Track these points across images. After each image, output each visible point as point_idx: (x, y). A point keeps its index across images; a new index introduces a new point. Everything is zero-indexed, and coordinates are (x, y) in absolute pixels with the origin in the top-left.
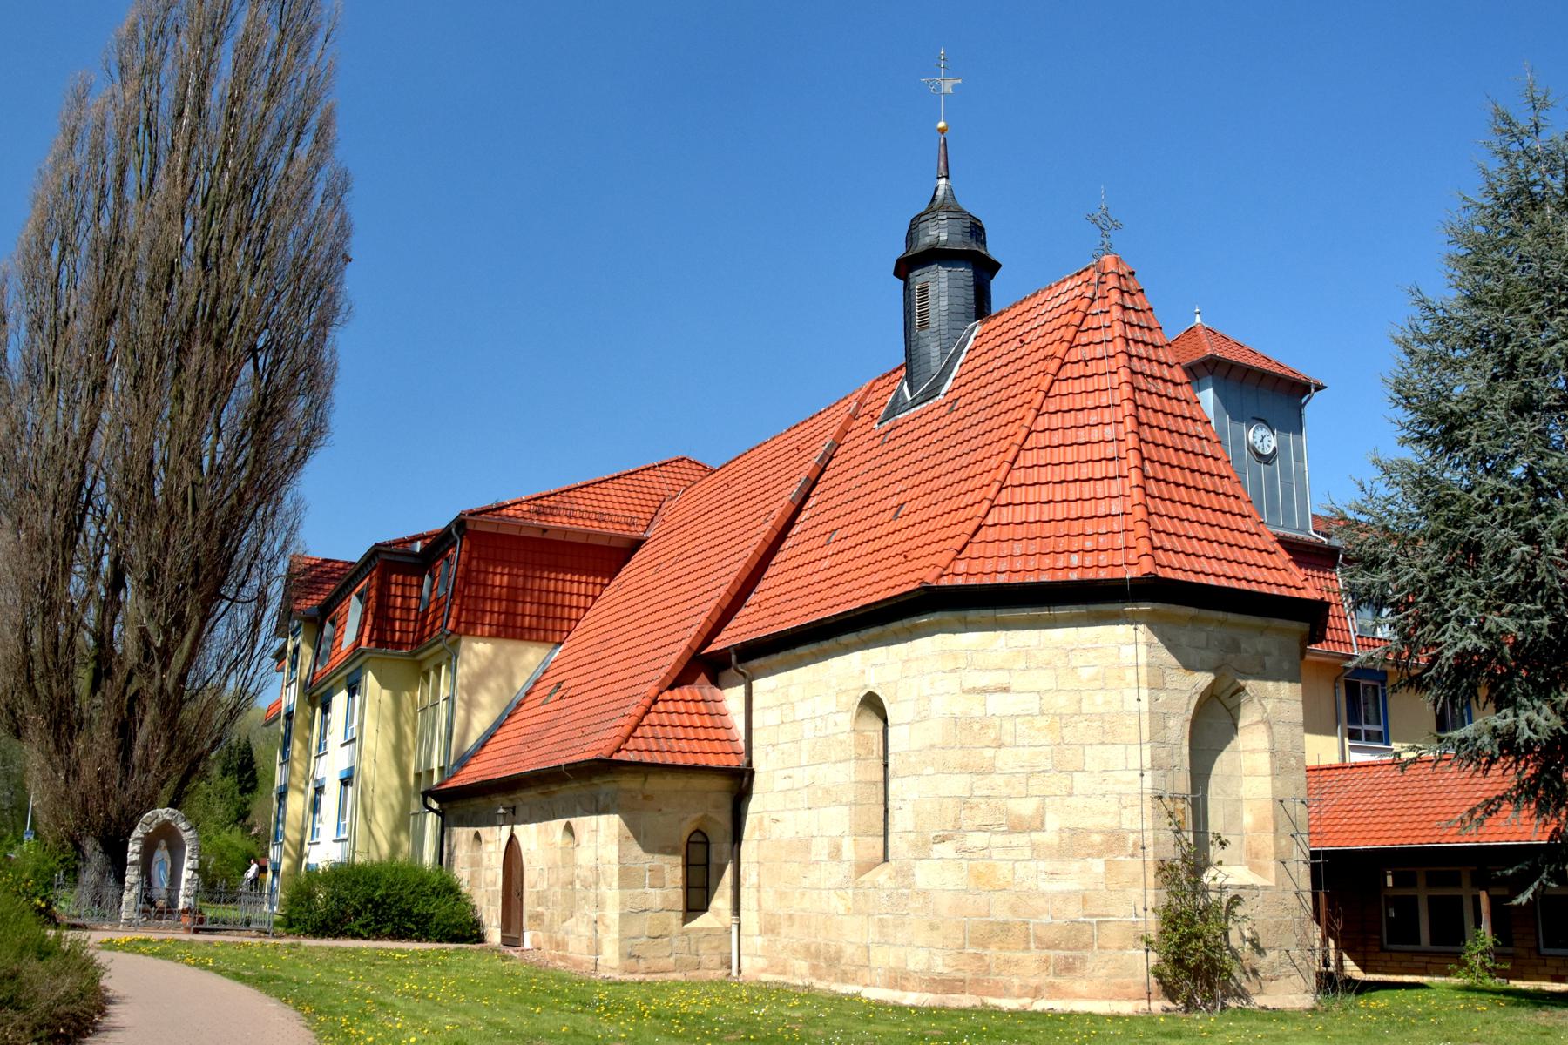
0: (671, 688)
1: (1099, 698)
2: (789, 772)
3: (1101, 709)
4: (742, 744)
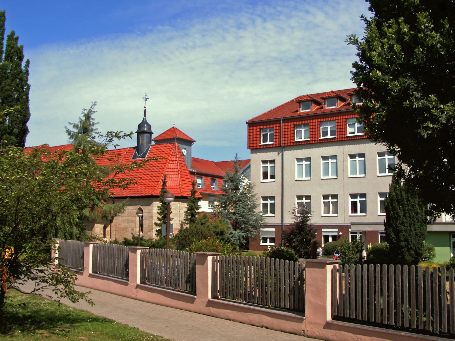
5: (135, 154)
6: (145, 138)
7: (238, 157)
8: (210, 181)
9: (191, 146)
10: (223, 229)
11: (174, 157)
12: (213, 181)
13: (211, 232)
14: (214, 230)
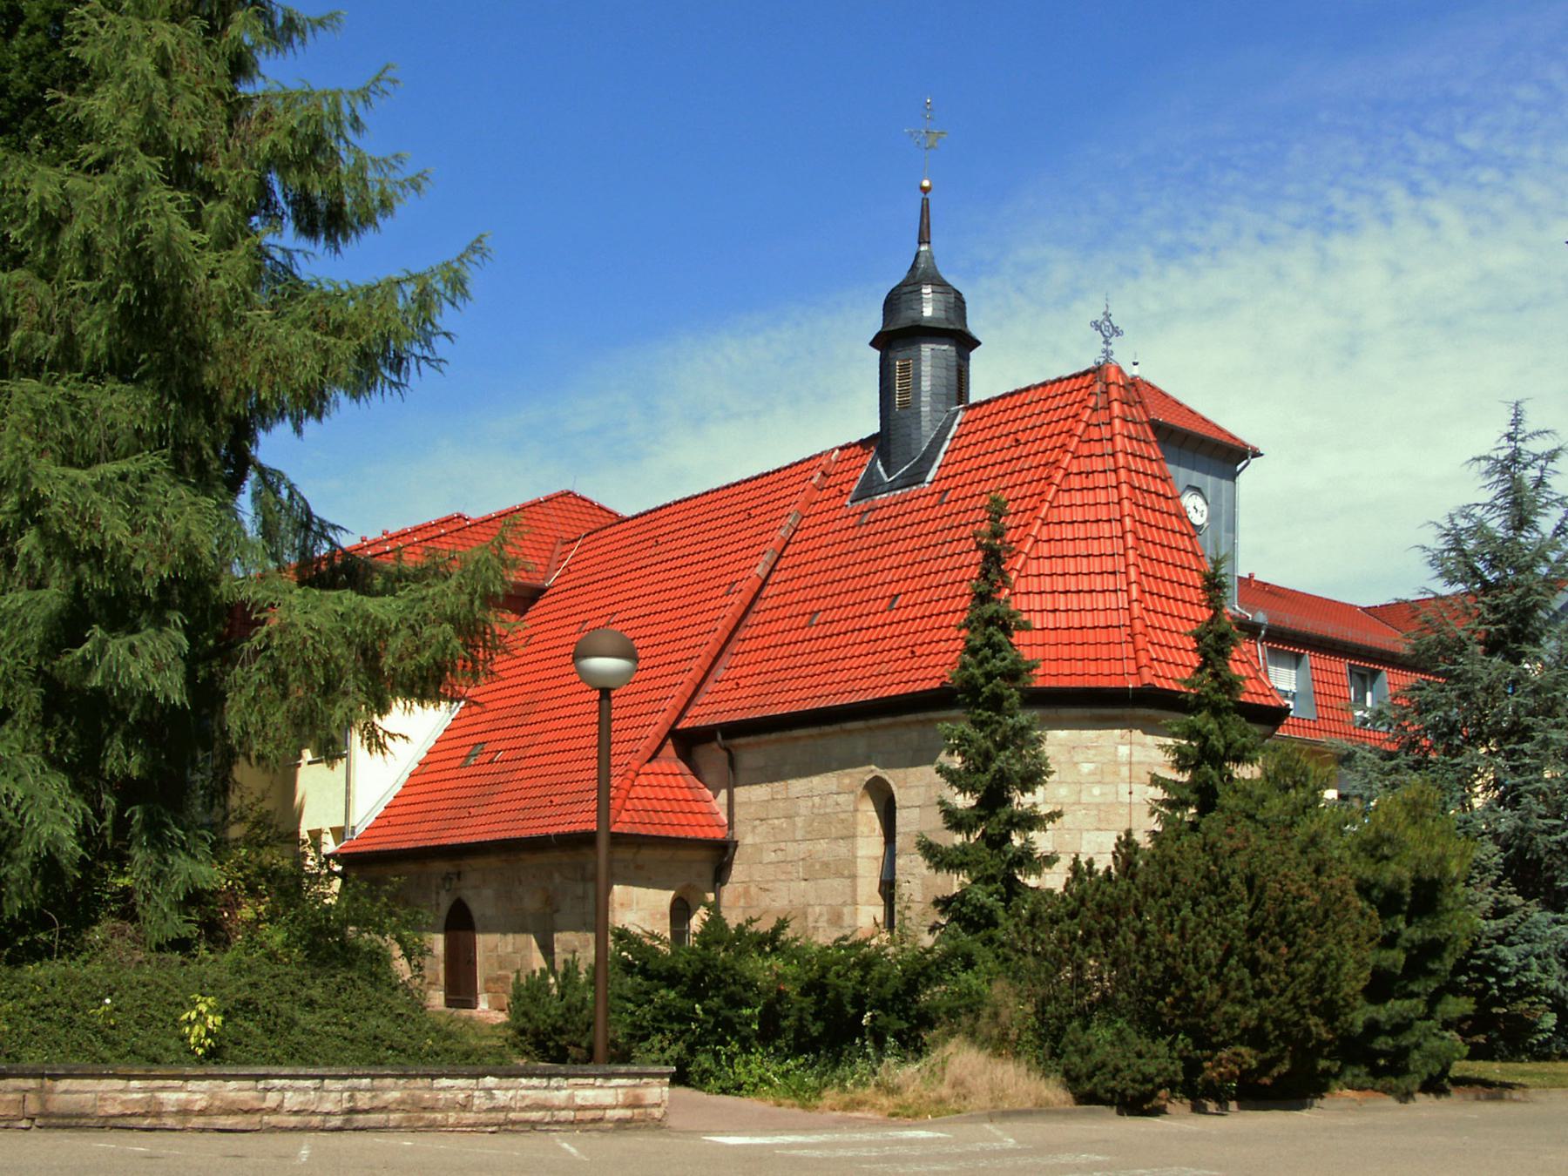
0: (649, 761)
1: (1096, 791)
2: (782, 845)
3: (1098, 800)
4: (724, 817)
5: (872, 470)
6: (926, 368)
7: (1528, 427)
8: (1346, 680)
9: (1233, 476)
10: (1442, 859)
11: (1097, 448)
12: (1365, 679)
13: (1340, 880)
14: (1366, 871)
